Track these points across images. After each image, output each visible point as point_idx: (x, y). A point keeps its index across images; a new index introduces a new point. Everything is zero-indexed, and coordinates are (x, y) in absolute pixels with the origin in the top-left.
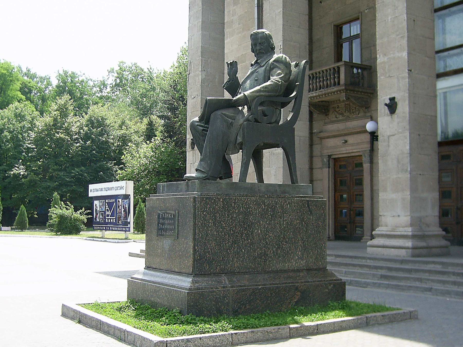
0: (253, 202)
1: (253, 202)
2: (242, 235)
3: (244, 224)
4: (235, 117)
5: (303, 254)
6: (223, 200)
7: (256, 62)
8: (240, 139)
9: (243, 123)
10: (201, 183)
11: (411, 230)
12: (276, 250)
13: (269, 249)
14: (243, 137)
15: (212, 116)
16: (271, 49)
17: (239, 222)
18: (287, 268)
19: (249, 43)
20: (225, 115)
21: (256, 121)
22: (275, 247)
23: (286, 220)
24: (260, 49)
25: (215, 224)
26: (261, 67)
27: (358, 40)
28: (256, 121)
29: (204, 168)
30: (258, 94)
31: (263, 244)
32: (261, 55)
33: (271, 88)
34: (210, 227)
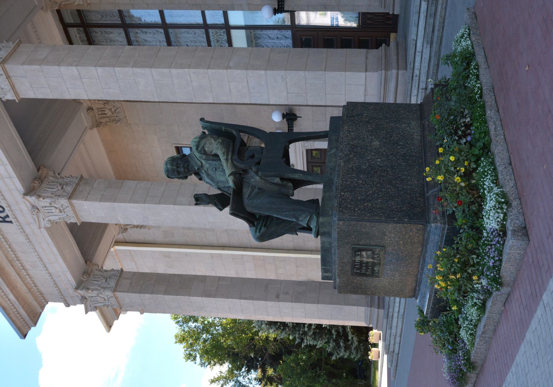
2: (382, 176)
3: (371, 174)
5: (405, 123)
7: (197, 174)
8: (277, 180)
9: (260, 177)
11: (377, 310)
12: (400, 145)
13: (398, 152)
14: (276, 176)
15: (249, 209)
17: (368, 178)
18: (419, 137)
20: (249, 196)
21: (258, 163)
22: (396, 147)
23: (367, 136)
25: (370, 201)
26: (202, 166)
27: (166, 12)
28: (258, 163)
29: (306, 217)
30: (230, 161)
31: (392, 157)
32: (190, 167)
34: (372, 205)
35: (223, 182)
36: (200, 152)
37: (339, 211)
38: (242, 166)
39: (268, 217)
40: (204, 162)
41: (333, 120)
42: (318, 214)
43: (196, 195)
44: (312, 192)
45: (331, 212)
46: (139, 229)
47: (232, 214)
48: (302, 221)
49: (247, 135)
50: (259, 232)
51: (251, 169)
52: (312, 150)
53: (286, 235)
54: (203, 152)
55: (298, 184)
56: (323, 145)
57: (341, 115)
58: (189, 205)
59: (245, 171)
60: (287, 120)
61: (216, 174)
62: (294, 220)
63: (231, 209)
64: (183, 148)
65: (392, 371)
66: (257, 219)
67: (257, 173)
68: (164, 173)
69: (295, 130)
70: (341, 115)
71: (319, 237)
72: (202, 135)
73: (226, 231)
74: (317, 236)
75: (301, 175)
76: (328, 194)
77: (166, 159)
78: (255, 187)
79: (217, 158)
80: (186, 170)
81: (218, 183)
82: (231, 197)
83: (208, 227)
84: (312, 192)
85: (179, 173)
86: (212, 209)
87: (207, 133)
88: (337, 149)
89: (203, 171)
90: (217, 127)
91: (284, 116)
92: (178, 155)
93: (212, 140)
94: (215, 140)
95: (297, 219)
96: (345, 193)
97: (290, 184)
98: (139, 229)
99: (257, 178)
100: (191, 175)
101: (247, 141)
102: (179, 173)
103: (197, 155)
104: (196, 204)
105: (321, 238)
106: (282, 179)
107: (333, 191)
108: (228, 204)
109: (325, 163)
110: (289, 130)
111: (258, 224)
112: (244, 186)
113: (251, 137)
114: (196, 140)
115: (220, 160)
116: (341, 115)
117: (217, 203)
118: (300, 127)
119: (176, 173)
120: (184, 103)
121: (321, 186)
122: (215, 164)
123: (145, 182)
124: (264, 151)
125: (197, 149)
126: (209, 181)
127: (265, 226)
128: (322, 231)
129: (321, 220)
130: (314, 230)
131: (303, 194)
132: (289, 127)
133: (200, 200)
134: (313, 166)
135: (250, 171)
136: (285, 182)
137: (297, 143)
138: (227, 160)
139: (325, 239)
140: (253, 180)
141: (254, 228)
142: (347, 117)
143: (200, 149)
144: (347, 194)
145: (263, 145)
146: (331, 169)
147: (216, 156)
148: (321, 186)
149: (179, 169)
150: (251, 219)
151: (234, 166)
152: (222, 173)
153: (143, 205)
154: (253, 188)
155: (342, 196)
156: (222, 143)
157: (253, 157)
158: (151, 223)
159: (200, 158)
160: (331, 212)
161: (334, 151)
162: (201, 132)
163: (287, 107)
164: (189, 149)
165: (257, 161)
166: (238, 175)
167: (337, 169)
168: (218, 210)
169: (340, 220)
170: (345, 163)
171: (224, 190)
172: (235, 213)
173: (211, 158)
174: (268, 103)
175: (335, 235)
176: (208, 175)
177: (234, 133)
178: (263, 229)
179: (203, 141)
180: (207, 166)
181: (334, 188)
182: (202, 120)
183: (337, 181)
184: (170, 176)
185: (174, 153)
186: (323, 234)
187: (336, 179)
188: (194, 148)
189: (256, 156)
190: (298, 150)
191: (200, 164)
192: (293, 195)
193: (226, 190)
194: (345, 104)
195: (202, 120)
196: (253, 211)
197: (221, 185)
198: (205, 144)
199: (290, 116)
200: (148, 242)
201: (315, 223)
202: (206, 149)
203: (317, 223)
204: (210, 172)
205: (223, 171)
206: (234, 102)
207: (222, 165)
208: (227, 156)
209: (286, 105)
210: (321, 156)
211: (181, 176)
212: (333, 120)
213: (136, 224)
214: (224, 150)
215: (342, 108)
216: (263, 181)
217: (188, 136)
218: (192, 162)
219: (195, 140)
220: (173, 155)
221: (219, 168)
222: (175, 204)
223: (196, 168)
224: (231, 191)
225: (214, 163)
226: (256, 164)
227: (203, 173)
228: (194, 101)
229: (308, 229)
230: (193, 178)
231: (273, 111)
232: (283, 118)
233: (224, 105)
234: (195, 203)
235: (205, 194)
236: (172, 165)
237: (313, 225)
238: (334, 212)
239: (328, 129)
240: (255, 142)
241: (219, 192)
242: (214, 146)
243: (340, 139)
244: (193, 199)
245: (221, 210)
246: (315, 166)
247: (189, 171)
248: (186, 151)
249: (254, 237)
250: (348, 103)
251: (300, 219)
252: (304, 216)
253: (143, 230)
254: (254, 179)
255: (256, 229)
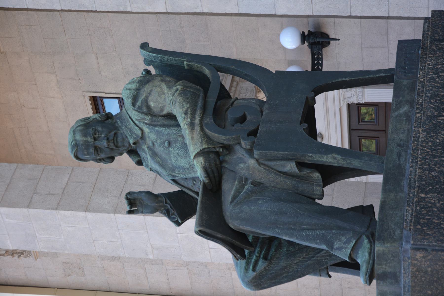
0: (432, 137)
1: (432, 137)
4: (241, 178)
6: (422, 192)
7: (133, 152)
8: (291, 167)
9: (257, 160)
10: (383, 240)
14: (288, 159)
15: (234, 224)
16: (109, 121)
19: (92, 166)
20: (234, 197)
21: (253, 133)
24: (108, 139)
26: (143, 137)
28: (253, 133)
29: (347, 242)
30: (197, 128)
33: (188, 103)
35: (183, 168)
36: (139, 110)
37: (416, 230)
38: (222, 138)
39: (272, 239)
40: (146, 130)
41: (404, 46)
42: (373, 235)
43: (129, 193)
44: (361, 190)
45: (398, 232)
46: (16, 257)
47: (201, 233)
48: (340, 249)
49: (230, 77)
50: (254, 270)
51: (240, 144)
52: (359, 105)
53: (307, 276)
54: (145, 110)
55: (330, 174)
56: (383, 94)
57: (419, 36)
58: (116, 211)
59: (228, 148)
60: (311, 45)
61: (169, 153)
62: (324, 247)
63: (200, 223)
64: (105, 100)
65: (266, 168)
66: (250, 245)
67: (250, 152)
68: (69, 149)
69: (328, 65)
70: (420, 37)
71: (374, 282)
72: (144, 77)
73: (187, 264)
74: (370, 279)
75: (339, 157)
76: (392, 196)
77: (73, 123)
78: (247, 179)
79: (173, 122)
80: (112, 145)
81: (173, 171)
82: (199, 198)
83: (151, 257)
84: (361, 190)
85: (97, 150)
86: (161, 221)
87: (153, 72)
88: (412, 106)
89: (145, 147)
90: (173, 60)
91: (304, 37)
92: (97, 116)
93: (164, 86)
94: (169, 87)
95: (331, 245)
96: (427, 193)
97: (317, 175)
98: (16, 257)
99: (252, 162)
100: (121, 154)
101: (231, 86)
102: (97, 150)
103: (135, 115)
104: (130, 212)
105: (378, 284)
106: (301, 165)
107: (402, 191)
108: (195, 214)
109: (385, 131)
110: (313, 65)
111: (251, 254)
112: (225, 177)
113: (237, 79)
114: (133, 86)
115: (178, 125)
116: (420, 37)
117: (172, 211)
118: (336, 59)
119: (92, 150)
120: (108, 12)
121: (379, 179)
122: (168, 134)
123: (30, 166)
124: (266, 107)
125: (134, 104)
126: (155, 166)
127: (265, 258)
128: (380, 271)
129: (378, 248)
130: (363, 268)
131: (339, 195)
132: (313, 60)
133: (136, 203)
134: (361, 138)
135: (237, 147)
136: (306, 172)
137: (330, 94)
138: (192, 125)
139: (386, 288)
140: (242, 165)
141: (244, 262)
142: (433, 41)
143: (139, 103)
144: (432, 197)
145: (262, 96)
146: (399, 145)
147: (171, 117)
148: (379, 179)
149: (98, 143)
150: (238, 243)
151: (207, 138)
152: (181, 152)
153: (25, 210)
154: (243, 181)
155: (421, 200)
156: (183, 93)
157: (243, 119)
158: (40, 247)
159: (139, 120)
160: (398, 232)
161: (405, 108)
162: (142, 70)
163: (310, 19)
164: (116, 101)
165: (251, 128)
166: (212, 156)
167: (412, 146)
168: (173, 225)
169: (418, 249)
170: (428, 133)
171: (185, 184)
172: (207, 231)
173: (161, 121)
174: (273, 13)
175: (406, 279)
176: (154, 155)
177: (207, 72)
178: (261, 265)
179: (146, 89)
180: (153, 136)
181: (405, 183)
182: (144, 46)
183: (411, 170)
184: (80, 156)
185: (88, 112)
186: (383, 277)
187: (408, 165)
188: (128, 102)
189: (249, 117)
190: (330, 105)
191: (139, 133)
192: (321, 198)
193: (189, 184)
194: (427, 14)
195: (144, 46)
196: (241, 227)
197: (180, 176)
198: (150, 94)
199: (316, 39)
200: (32, 283)
201: (367, 254)
202: (152, 104)
203: (370, 254)
204: (159, 149)
205: (185, 146)
206: (206, 11)
207: (182, 136)
208: (193, 117)
209: (308, 16)
210: (377, 116)
211: (103, 156)
212: (404, 46)
213: (11, 248)
214: (186, 106)
215: (422, 22)
216: (262, 169)
217: (116, 75)
218: (123, 130)
219: (130, 86)
220: (86, 116)
221: (176, 142)
222: (87, 210)
223: (132, 141)
224: (199, 188)
225: (166, 131)
226: (249, 135)
227: (143, 150)
228: (129, 9)
229: (351, 266)
230: (124, 160)
231: (282, 28)
232: (303, 42)
233: (186, 17)
234: (128, 209)
235: (149, 193)
236: (85, 135)
237: (362, 258)
238: (405, 232)
239: (392, 65)
240: (245, 91)
241: (175, 188)
242: (168, 98)
243: (419, 86)
244: (125, 202)
245: (178, 224)
246: (366, 138)
247: (117, 146)
248: (112, 107)
249: (243, 281)
250: (434, 12)
251: (337, 245)
252: (343, 239)
253: (23, 260)
254: (246, 164)
255: (248, 264)
